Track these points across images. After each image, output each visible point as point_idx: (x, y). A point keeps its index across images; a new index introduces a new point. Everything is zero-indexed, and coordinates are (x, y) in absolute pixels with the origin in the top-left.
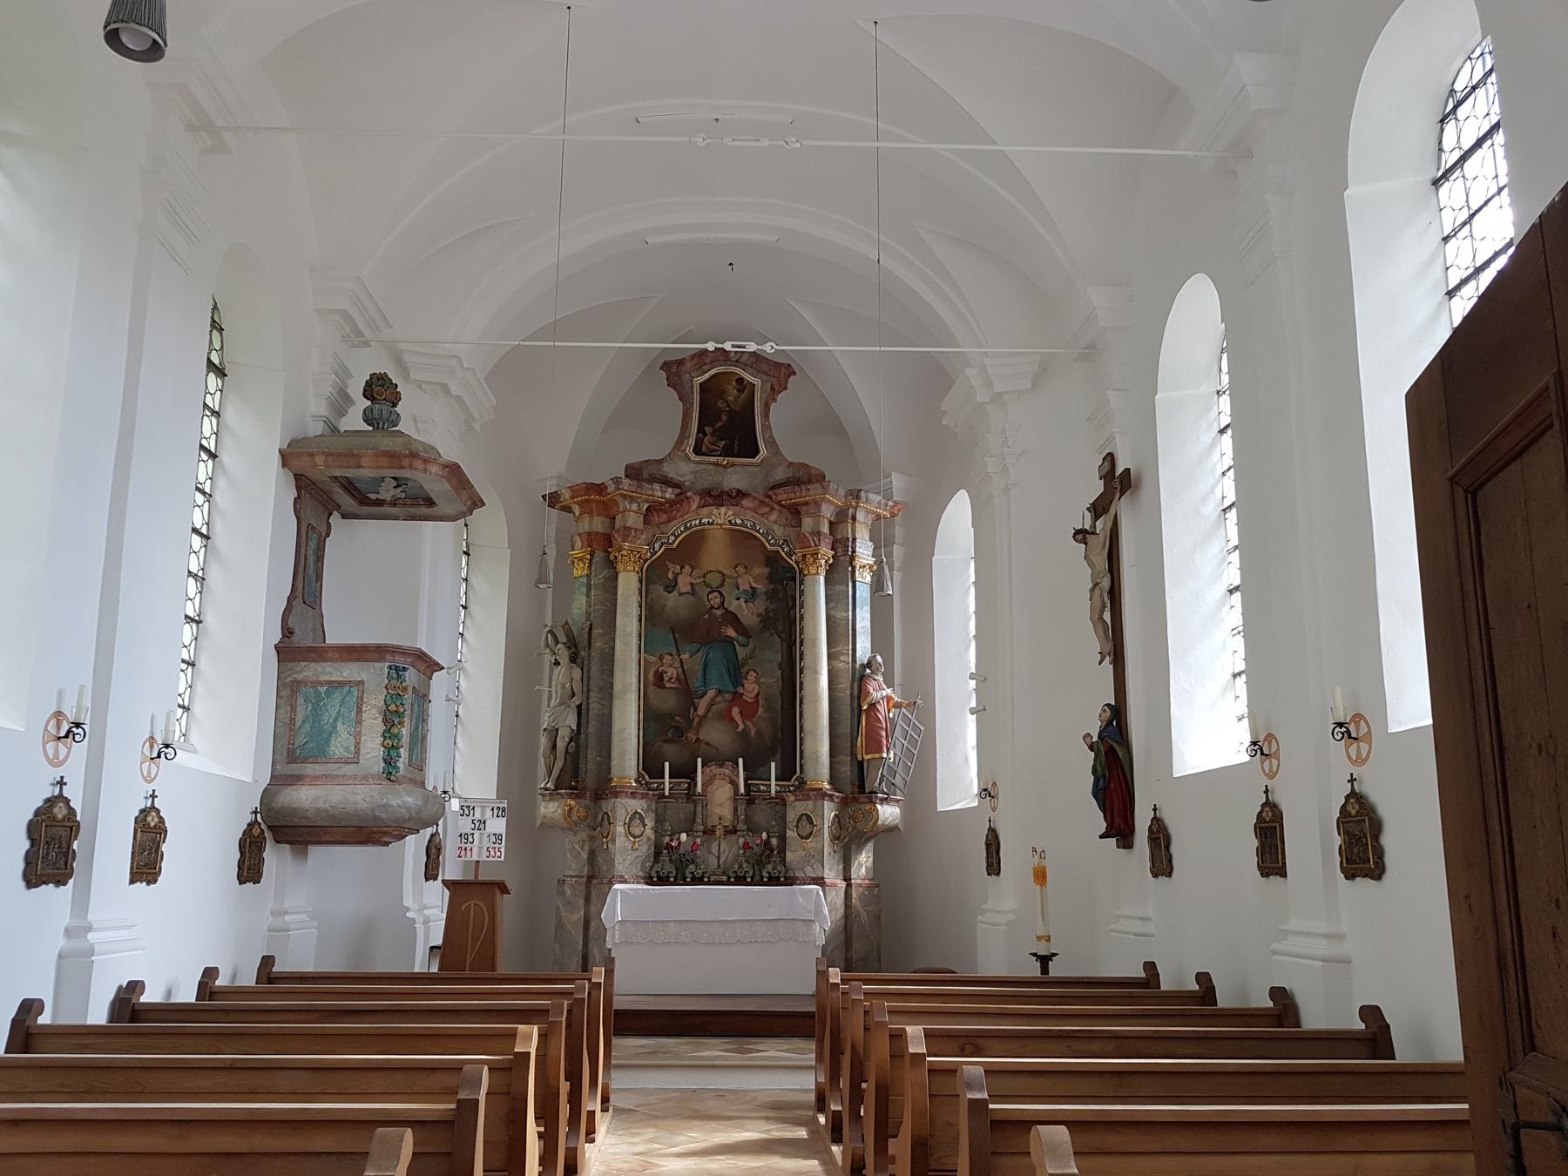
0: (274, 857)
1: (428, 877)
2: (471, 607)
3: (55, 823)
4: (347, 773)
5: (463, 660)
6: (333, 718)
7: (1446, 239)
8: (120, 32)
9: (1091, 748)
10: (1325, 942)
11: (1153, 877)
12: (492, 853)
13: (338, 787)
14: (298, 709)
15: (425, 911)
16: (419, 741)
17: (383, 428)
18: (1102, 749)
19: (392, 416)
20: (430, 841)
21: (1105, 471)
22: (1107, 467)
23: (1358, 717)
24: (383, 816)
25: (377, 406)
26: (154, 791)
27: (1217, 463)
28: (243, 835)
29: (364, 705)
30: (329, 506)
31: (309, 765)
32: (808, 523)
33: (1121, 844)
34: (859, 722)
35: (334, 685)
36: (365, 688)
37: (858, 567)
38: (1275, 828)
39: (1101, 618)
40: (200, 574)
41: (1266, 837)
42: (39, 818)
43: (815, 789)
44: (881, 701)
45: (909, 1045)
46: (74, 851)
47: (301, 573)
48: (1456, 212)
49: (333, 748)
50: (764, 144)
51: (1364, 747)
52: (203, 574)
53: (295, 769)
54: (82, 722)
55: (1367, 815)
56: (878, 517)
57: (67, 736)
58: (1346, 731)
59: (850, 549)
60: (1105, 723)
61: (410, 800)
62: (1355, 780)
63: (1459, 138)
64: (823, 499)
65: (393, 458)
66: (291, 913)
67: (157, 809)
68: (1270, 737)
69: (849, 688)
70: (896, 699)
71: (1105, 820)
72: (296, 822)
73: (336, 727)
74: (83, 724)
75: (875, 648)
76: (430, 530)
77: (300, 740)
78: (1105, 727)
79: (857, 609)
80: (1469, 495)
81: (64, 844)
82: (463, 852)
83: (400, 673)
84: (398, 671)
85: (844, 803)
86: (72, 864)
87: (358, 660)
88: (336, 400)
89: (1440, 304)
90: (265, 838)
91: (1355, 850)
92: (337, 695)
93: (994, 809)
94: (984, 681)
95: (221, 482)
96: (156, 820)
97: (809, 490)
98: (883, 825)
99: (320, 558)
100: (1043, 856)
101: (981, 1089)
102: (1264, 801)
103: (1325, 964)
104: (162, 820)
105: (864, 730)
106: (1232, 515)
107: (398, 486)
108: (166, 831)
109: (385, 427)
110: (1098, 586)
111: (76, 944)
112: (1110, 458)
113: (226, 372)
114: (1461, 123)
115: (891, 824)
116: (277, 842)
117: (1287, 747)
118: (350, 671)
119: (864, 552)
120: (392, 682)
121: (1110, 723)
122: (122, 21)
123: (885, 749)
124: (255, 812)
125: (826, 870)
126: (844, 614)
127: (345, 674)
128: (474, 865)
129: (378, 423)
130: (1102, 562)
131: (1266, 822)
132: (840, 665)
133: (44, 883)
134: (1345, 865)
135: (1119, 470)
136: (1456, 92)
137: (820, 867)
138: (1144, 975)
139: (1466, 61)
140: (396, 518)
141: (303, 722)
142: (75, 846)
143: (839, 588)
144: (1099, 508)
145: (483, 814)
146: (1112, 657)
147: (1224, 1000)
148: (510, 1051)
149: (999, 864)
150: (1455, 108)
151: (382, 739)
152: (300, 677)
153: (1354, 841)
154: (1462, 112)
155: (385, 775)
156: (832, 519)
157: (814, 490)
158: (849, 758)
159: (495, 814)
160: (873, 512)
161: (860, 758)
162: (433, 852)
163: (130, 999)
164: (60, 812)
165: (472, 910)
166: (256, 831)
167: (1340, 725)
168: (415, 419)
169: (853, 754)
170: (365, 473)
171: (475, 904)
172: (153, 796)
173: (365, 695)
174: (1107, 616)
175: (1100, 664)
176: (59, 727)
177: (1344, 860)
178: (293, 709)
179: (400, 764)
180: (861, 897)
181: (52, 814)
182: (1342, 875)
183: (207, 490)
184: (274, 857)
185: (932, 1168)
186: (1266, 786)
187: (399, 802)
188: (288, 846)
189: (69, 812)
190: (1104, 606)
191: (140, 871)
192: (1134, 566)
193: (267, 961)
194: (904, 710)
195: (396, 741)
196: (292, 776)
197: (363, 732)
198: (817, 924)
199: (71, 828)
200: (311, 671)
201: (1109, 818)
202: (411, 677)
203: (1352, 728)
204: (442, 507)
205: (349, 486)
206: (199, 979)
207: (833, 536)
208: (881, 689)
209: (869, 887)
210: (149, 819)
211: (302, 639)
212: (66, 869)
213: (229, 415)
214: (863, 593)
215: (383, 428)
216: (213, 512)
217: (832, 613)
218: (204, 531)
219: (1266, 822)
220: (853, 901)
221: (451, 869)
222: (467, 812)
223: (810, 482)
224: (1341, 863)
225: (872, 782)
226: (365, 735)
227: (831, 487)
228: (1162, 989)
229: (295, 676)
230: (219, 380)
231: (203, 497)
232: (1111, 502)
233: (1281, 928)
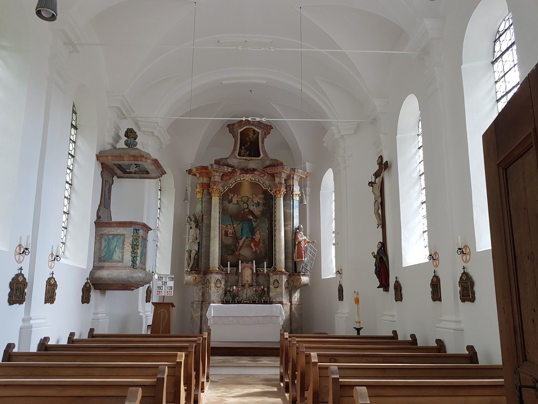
0: (94, 295)
1: (147, 301)
2: (162, 209)
3: (19, 283)
4: (119, 266)
5: (159, 227)
6: (114, 247)
7: (496, 82)
8: (41, 11)
9: (374, 257)
10: (455, 324)
11: (396, 301)
12: (169, 293)
13: (116, 270)
14: (102, 244)
15: (146, 313)
16: (144, 254)
17: (131, 147)
18: (378, 257)
19: (135, 143)
20: (147, 289)
21: (379, 162)
22: (380, 160)
23: (466, 246)
24: (131, 280)
25: (129, 140)
26: (53, 272)
27: (418, 159)
28: (84, 287)
29: (125, 242)
30: (113, 174)
31: (106, 263)
32: (277, 180)
33: (385, 290)
34: (295, 248)
35: (115, 235)
36: (125, 236)
37: (294, 195)
38: (438, 284)
39: (378, 212)
40: (69, 197)
41: (434, 288)
42: (14, 281)
43: (280, 271)
44: (302, 241)
45: (312, 359)
46: (25, 292)
47: (103, 197)
48: (500, 73)
49: (114, 257)
50: (262, 50)
51: (468, 257)
52: (70, 197)
53: (101, 264)
54: (28, 248)
55: (469, 280)
56: (301, 178)
57: (23, 253)
58: (462, 251)
59: (292, 189)
60: (379, 248)
61: (141, 275)
62: (465, 268)
63: (501, 47)
64: (282, 171)
65: (135, 157)
66: (100, 314)
67: (54, 278)
68: (436, 253)
69: (291, 236)
70: (307, 240)
71: (379, 282)
72: (101, 282)
73: (115, 250)
74: (29, 249)
75: (300, 223)
76: (147, 182)
77: (103, 254)
78: (379, 250)
79: (294, 209)
80: (504, 170)
81: (22, 290)
82: (159, 293)
83: (137, 231)
84: (137, 230)
85: (290, 276)
86: (25, 297)
87: (123, 227)
88: (115, 137)
89: (494, 104)
90: (91, 288)
91: (465, 292)
92: (116, 239)
93: (341, 278)
94: (338, 234)
95: (76, 166)
96: (54, 282)
97: (277, 168)
98: (303, 283)
99: (110, 192)
100: (358, 294)
101: (336, 374)
102: (434, 275)
103: (455, 331)
104: (55, 282)
105: (296, 251)
106: (423, 177)
107: (137, 167)
108: (57, 285)
109: (132, 147)
110: (377, 201)
111: (26, 324)
112: (381, 157)
113: (77, 128)
114: (501, 42)
115: (306, 283)
116: (95, 289)
117: (441, 256)
118: (120, 230)
119: (297, 190)
120: (134, 234)
121: (381, 248)
122: (42, 7)
123: (304, 257)
124: (88, 279)
125: (284, 299)
126: (289, 211)
127: (118, 232)
128: (163, 297)
129: (130, 145)
130: (378, 193)
131: (434, 282)
132: (288, 228)
133: (15, 303)
134: (461, 297)
135: (384, 162)
136: (499, 32)
137: (281, 298)
138: (392, 335)
139: (503, 21)
140: (136, 178)
141: (104, 248)
142: (26, 290)
143: (288, 202)
144: (377, 175)
145: (166, 280)
146: (381, 226)
147: (420, 344)
148: (175, 361)
149: (343, 297)
150: (499, 37)
151: (131, 254)
152: (103, 233)
153: (464, 289)
154: (502, 38)
155: (132, 266)
156: (285, 178)
157: (279, 168)
158: (291, 261)
159: (170, 280)
160: (299, 176)
161: (295, 260)
162: (149, 293)
163: (45, 343)
164: (20, 279)
165: (162, 313)
166: (88, 285)
167: (460, 249)
168: (142, 144)
169: (293, 259)
170: (125, 162)
171: (163, 311)
172: (53, 274)
173: (125, 239)
174: (380, 212)
175: (377, 228)
176: (20, 250)
177: (461, 296)
178: (101, 243)
179: (137, 263)
180: (295, 308)
181: (18, 280)
182: (461, 301)
183: (71, 168)
184: (94, 295)
185: (320, 401)
186: (435, 270)
187: (137, 275)
188: (99, 291)
189: (24, 279)
190: (379, 208)
191: (48, 299)
192: (389, 194)
193: (92, 330)
194: (310, 244)
195: (136, 255)
196: (100, 266)
197: (124, 252)
198: (280, 317)
199: (24, 284)
200: (107, 230)
201: (380, 281)
202: (141, 232)
203: (464, 250)
204: (152, 174)
205: (120, 167)
206: (68, 336)
207: (286, 184)
208: (302, 237)
209: (298, 305)
210: (51, 281)
211: (104, 219)
212: (23, 299)
213: (79, 143)
214: (296, 204)
215: (131, 147)
216: (73, 176)
217: (285, 210)
218: (70, 182)
219: (434, 282)
220: (293, 309)
221: (155, 298)
222: (160, 279)
223: (278, 166)
224: (460, 296)
225: (299, 269)
226: (125, 252)
227: (285, 167)
228: (399, 340)
229: (101, 232)
230: (75, 130)
231: (70, 171)
232: (381, 172)
233: (439, 319)
